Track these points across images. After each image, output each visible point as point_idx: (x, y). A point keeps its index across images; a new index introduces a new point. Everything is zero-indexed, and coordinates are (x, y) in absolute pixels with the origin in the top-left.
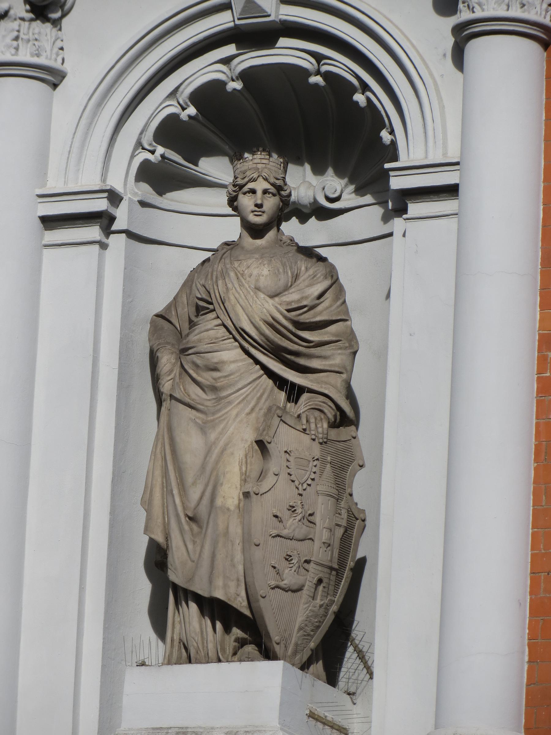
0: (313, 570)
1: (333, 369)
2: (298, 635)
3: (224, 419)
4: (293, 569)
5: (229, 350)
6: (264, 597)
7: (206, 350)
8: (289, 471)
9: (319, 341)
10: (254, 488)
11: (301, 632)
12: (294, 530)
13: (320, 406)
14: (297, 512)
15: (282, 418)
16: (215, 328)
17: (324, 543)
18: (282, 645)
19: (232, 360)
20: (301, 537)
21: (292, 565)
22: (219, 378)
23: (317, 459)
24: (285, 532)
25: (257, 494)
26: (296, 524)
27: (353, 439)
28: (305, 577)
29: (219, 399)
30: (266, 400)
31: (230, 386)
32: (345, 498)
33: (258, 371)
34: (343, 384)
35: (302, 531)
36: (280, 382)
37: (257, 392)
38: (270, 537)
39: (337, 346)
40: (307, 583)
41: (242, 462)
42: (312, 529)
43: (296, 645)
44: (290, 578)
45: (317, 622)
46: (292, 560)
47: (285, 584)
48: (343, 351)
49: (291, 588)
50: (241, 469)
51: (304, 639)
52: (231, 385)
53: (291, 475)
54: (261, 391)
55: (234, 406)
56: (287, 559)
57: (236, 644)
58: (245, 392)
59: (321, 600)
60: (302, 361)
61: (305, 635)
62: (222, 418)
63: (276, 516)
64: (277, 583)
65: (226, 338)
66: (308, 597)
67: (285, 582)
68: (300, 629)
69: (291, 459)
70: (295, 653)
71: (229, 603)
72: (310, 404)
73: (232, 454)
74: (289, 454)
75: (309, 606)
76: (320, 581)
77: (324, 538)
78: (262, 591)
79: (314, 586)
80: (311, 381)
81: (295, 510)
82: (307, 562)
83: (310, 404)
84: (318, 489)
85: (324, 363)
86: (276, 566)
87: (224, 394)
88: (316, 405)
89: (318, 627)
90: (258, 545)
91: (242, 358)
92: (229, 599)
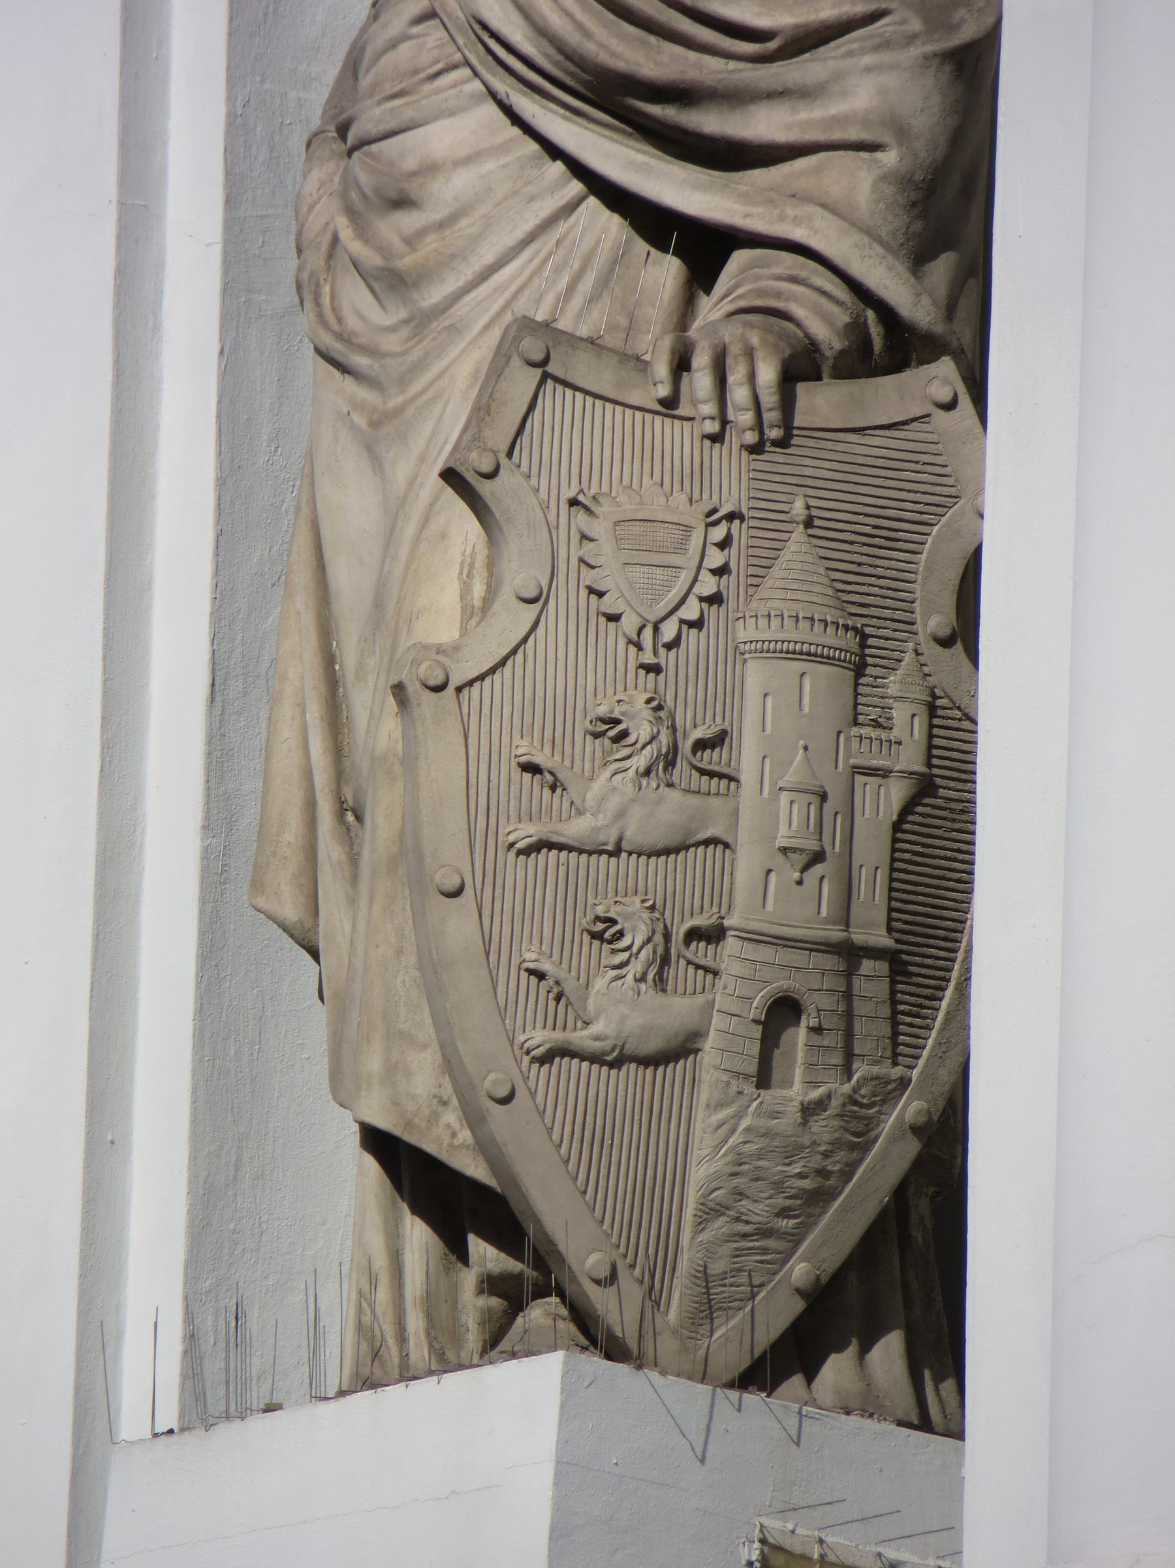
0: (736, 968)
1: (837, 136)
2: (704, 1237)
3: (435, 399)
4: (635, 968)
5: (452, 113)
6: (506, 1100)
7: (383, 128)
8: (588, 577)
9: (797, 27)
10: (423, 667)
11: (720, 1226)
12: (621, 814)
13: (778, 295)
14: (631, 739)
15: (551, 368)
16: (415, 30)
17: (785, 850)
18: (630, 1287)
19: (462, 152)
20: (658, 838)
21: (626, 955)
22: (421, 233)
23: (731, 517)
24: (574, 829)
25: (439, 689)
26: (629, 789)
27: (940, 416)
28: (700, 999)
29: (421, 321)
30: (592, 299)
31: (451, 259)
32: (908, 657)
33: (559, 185)
34: (889, 190)
35: (667, 810)
36: (654, 223)
37: (558, 270)
38: (512, 854)
39: (872, 36)
40: (717, 1021)
41: (472, 565)
42: (714, 802)
43: (704, 1275)
44: (618, 1008)
45: (801, 1176)
46: (620, 934)
47: (597, 1038)
48: (887, 57)
49: (630, 1049)
50: (466, 589)
51: (738, 1253)
52: (453, 256)
53: (601, 595)
54: (576, 264)
55: (471, 343)
56: (597, 936)
57: (495, 1302)
58: (514, 278)
59: (812, 1084)
60: (710, 122)
61: (745, 1236)
62: (425, 397)
63: (532, 768)
64: (559, 1036)
65: (440, 66)
66: (725, 1077)
67: (596, 1028)
68: (709, 1212)
69: (599, 528)
70: (706, 1310)
71: (406, 1137)
72: (741, 291)
73: (444, 535)
74: (587, 509)
75: (739, 1116)
76: (784, 1011)
77: (783, 829)
78: (492, 1077)
79: (757, 1031)
80: (745, 198)
81: (624, 734)
82: (714, 935)
83: (741, 291)
84: (742, 635)
85: (803, 115)
86: (546, 966)
87: (433, 295)
88: (762, 293)
89: (819, 1198)
90: (457, 893)
91: (499, 140)
92: (409, 1124)
